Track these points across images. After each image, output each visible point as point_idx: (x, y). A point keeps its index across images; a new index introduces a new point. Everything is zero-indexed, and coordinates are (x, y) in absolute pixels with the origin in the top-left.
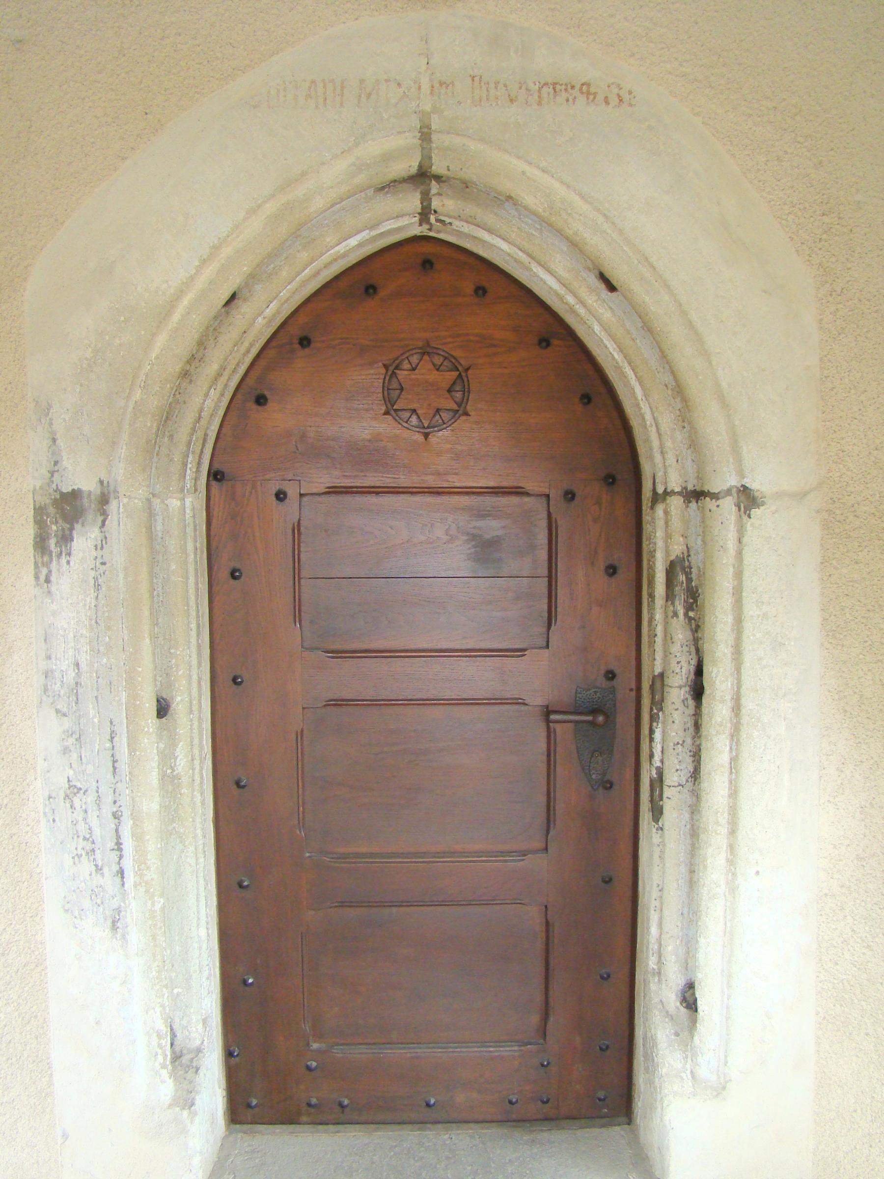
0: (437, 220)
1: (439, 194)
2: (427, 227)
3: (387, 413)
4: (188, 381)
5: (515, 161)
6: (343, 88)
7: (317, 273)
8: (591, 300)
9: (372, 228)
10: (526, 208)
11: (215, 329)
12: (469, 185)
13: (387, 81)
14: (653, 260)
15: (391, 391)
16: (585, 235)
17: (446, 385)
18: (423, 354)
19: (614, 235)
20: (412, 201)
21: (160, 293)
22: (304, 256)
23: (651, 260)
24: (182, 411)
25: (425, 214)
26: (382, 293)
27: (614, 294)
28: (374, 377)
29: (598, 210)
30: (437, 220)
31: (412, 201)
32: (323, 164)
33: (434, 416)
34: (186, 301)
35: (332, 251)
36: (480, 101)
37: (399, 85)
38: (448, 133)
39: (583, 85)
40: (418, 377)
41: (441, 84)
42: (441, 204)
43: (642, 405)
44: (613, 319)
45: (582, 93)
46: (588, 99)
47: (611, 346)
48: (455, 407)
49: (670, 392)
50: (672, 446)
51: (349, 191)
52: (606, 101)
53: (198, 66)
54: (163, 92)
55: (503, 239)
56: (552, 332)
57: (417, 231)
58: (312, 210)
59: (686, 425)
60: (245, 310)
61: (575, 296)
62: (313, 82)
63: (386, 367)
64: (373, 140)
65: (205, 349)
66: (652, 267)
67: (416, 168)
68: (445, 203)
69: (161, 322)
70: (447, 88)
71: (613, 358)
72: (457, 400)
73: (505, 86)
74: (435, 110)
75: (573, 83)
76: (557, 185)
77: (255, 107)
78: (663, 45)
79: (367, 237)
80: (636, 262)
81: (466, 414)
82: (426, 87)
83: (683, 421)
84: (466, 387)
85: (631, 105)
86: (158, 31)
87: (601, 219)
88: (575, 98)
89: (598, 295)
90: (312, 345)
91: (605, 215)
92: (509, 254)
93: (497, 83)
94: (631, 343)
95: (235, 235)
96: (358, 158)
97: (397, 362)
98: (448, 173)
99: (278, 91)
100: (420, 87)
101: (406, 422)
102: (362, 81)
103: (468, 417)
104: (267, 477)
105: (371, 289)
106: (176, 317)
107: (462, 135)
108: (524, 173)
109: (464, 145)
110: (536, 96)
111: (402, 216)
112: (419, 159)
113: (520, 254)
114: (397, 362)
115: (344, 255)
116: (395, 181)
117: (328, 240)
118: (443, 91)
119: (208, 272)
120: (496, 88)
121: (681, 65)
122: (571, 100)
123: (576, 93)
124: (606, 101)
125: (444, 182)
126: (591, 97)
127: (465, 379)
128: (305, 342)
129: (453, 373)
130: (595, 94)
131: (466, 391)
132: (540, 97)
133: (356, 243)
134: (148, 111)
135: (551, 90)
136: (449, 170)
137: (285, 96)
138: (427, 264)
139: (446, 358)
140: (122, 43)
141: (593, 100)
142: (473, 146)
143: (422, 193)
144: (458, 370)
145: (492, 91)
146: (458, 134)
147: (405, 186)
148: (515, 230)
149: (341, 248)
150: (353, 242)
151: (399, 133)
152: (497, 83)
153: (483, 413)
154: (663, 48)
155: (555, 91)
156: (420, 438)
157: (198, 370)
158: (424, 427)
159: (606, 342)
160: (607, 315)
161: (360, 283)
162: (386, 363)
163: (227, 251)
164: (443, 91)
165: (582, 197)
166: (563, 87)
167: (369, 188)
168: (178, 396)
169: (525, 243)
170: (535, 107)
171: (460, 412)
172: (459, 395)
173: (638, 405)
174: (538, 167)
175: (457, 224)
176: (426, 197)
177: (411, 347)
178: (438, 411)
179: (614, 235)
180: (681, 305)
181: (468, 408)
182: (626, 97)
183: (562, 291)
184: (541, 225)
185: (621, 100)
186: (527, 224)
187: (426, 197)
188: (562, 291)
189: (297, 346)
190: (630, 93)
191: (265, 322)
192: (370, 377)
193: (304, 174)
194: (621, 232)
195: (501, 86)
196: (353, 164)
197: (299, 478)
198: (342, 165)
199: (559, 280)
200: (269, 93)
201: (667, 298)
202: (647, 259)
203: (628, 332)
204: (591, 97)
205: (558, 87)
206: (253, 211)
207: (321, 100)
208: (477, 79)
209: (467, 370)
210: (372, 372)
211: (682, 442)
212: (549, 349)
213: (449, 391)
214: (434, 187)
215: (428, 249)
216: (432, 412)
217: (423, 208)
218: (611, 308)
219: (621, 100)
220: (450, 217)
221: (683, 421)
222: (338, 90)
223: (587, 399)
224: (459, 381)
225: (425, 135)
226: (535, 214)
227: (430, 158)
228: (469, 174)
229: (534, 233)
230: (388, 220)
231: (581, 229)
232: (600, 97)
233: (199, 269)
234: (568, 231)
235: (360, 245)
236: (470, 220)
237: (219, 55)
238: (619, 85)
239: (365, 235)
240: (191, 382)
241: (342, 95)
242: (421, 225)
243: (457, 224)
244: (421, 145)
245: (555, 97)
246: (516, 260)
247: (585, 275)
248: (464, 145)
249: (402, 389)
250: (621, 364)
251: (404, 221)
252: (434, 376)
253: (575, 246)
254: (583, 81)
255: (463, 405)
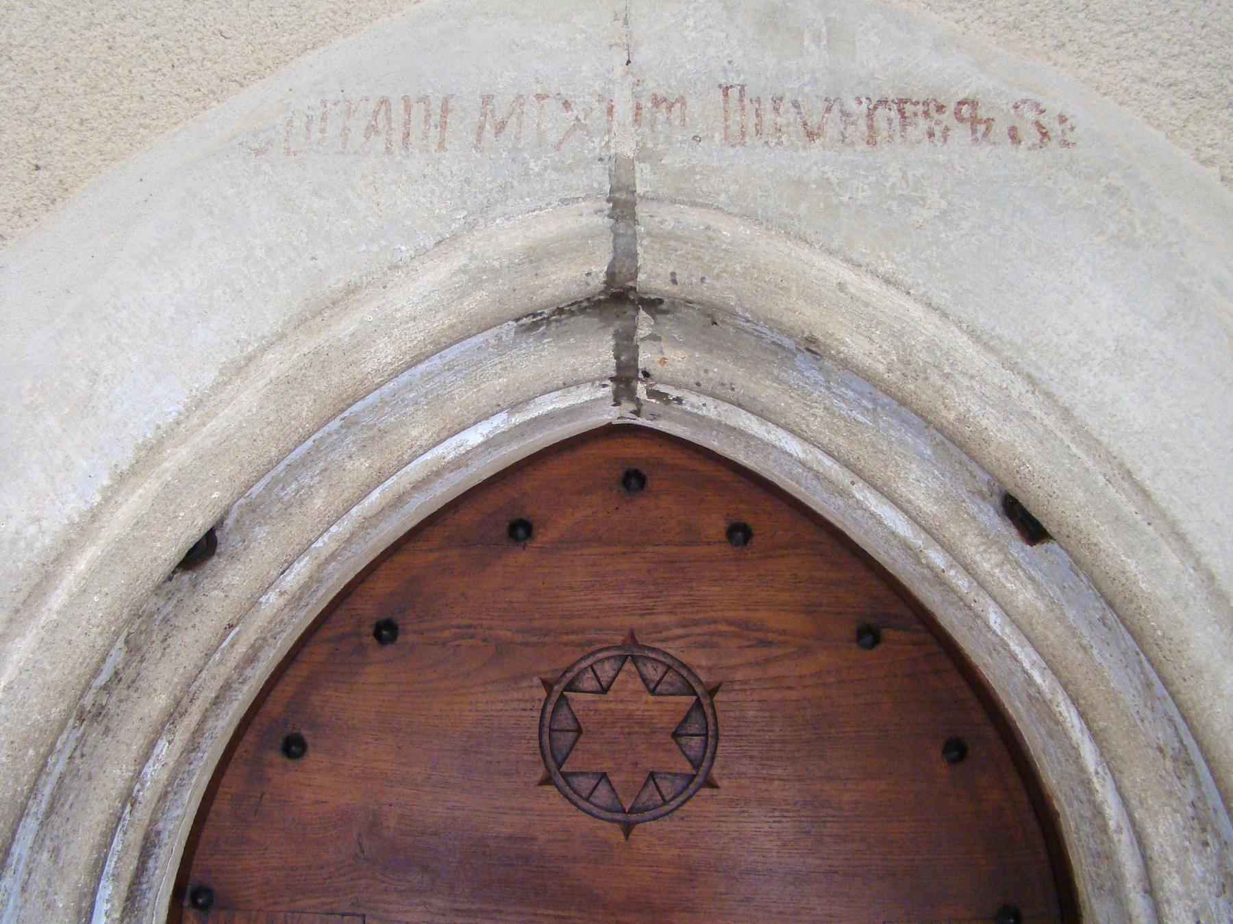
0: (652, 394)
1: (654, 338)
2: (632, 407)
3: (547, 781)
4: (101, 728)
5: (821, 261)
6: (445, 111)
7: (399, 500)
8: (987, 563)
9: (514, 407)
10: (845, 364)
11: (166, 620)
12: (719, 317)
13: (540, 97)
14: (1144, 475)
15: (555, 735)
16: (985, 423)
17: (669, 722)
18: (624, 659)
19: (1050, 422)
20: (596, 352)
21: (22, 544)
22: (362, 466)
23: (1138, 477)
24: (83, 796)
25: (625, 379)
26: (543, 537)
27: (1039, 548)
28: (522, 705)
29: (1013, 367)
30: (652, 394)
31: (596, 352)
32: (394, 267)
33: (645, 785)
34: (82, 564)
35: (428, 456)
36: (743, 134)
37: (567, 105)
38: (673, 202)
39: (961, 103)
40: (612, 706)
41: (656, 101)
42: (658, 358)
43: (1097, 784)
44: (1039, 604)
45: (961, 120)
46: (974, 131)
47: (1026, 656)
48: (688, 768)
49: (1169, 764)
50: (1181, 889)
51: (452, 327)
52: (1014, 136)
53: (152, 76)
54: (76, 126)
55: (792, 432)
56: (889, 624)
57: (611, 414)
58: (370, 367)
59: (1209, 838)
60: (229, 580)
61: (947, 548)
62: (384, 101)
63: (548, 685)
64: (507, 217)
65: (141, 661)
66: (1146, 494)
67: (602, 277)
68: (666, 356)
69: (17, 611)
70: (669, 109)
71: (1030, 680)
72: (692, 753)
73: (796, 105)
74: (644, 154)
75: (941, 101)
76: (917, 311)
77: (258, 152)
78: (1123, 27)
79: (504, 427)
80: (1101, 480)
81: (710, 784)
82: (624, 109)
83: (1204, 830)
84: (711, 727)
85: (1065, 144)
86: (83, 13)
87: (1019, 386)
88: (947, 129)
89: (1003, 550)
90: (400, 639)
91: (1030, 379)
92: (803, 463)
93: (777, 101)
94: (1080, 655)
95: (195, 421)
96: (473, 257)
97: (569, 675)
98: (675, 289)
99: (310, 120)
100: (610, 111)
101: (587, 799)
102: (487, 99)
103: (715, 791)
104: (300, 904)
105: (520, 530)
106: (58, 599)
107: (702, 206)
108: (841, 287)
109: (708, 228)
110: (863, 125)
111: (577, 383)
112: (609, 258)
113: (828, 462)
114: (569, 675)
115: (459, 463)
116: (560, 311)
117: (414, 433)
118: (662, 116)
119: (134, 502)
120: (776, 110)
121: (1164, 65)
122: (938, 134)
123: (947, 118)
124: (1014, 136)
125: (666, 312)
126: (981, 128)
127: (709, 712)
128: (386, 631)
129: (684, 699)
130: (989, 121)
131: (711, 736)
132: (871, 127)
133: (480, 439)
134: (40, 163)
135: (894, 114)
136: (674, 282)
137: (323, 131)
138: (633, 480)
139: (669, 668)
140: (9, 36)
141: (985, 135)
142: (727, 229)
143: (616, 335)
144: (695, 694)
145: (768, 116)
146: (694, 204)
147: (581, 319)
148: (820, 412)
149: (448, 450)
150: (473, 437)
151: (564, 202)
152: (777, 101)
153: (744, 782)
154: (1122, 33)
155: (903, 116)
156: (614, 833)
157: (123, 707)
158: (624, 811)
159: (1014, 647)
160: (1025, 596)
161: (498, 514)
162: (548, 676)
163: (177, 457)
164: (662, 116)
165: (974, 334)
166: (920, 108)
167: (499, 322)
168: (78, 761)
169: (841, 441)
170: (862, 146)
171: (698, 780)
172: (696, 742)
173: (1086, 784)
174: (874, 274)
175: (692, 401)
176: (626, 343)
177: (598, 646)
178: (652, 776)
179: (1050, 422)
180: (1212, 578)
181: (715, 772)
182: (1055, 128)
183: (917, 540)
184: (874, 401)
185: (1045, 135)
186: (843, 399)
187: (626, 343)
188: (917, 540)
189: (370, 640)
190: (1062, 119)
191: (282, 601)
192: (515, 705)
193: (352, 290)
194: (1066, 414)
195: (786, 106)
196: (464, 270)
197: (361, 911)
198: (437, 274)
199: (914, 518)
200: (290, 123)
201: (1175, 561)
202: (1128, 475)
203: (1073, 631)
204: (981, 128)
205: (909, 108)
206: (239, 369)
207: (397, 137)
208: (734, 93)
209: (712, 692)
210: (517, 695)
211: (1203, 880)
212: (880, 647)
213: (675, 735)
214: (645, 324)
215: (635, 450)
216: (641, 778)
217: (620, 367)
218: (1032, 579)
219: (1045, 135)
220: (678, 386)
221: (1204, 830)
222: (436, 118)
223: (956, 750)
224: (696, 716)
225: (623, 207)
226: (869, 378)
227: (634, 255)
228: (718, 290)
229: (860, 418)
230: (545, 392)
231: (975, 408)
232: (1000, 129)
233: (110, 497)
234: (945, 413)
235: (490, 444)
236: (720, 391)
237: (196, 54)
238: (1037, 105)
239: (499, 423)
240: (107, 730)
241: (443, 125)
242: (617, 403)
243: (692, 401)
244: (613, 229)
245: (904, 127)
246: (817, 475)
247: (973, 509)
248: (708, 228)
249: (579, 731)
250: (1049, 696)
251: (583, 395)
252: (646, 705)
253: (956, 446)
254: (961, 97)
255: (705, 764)
